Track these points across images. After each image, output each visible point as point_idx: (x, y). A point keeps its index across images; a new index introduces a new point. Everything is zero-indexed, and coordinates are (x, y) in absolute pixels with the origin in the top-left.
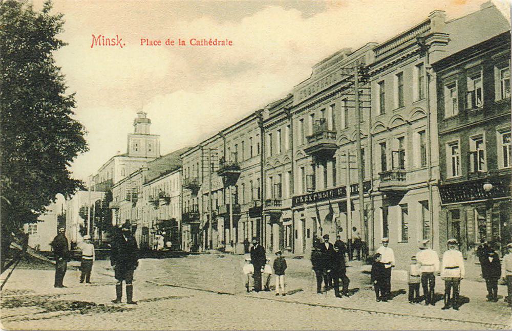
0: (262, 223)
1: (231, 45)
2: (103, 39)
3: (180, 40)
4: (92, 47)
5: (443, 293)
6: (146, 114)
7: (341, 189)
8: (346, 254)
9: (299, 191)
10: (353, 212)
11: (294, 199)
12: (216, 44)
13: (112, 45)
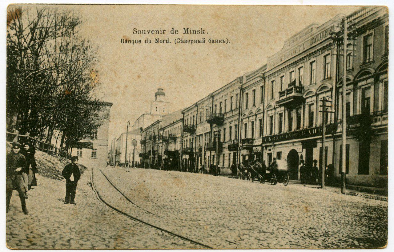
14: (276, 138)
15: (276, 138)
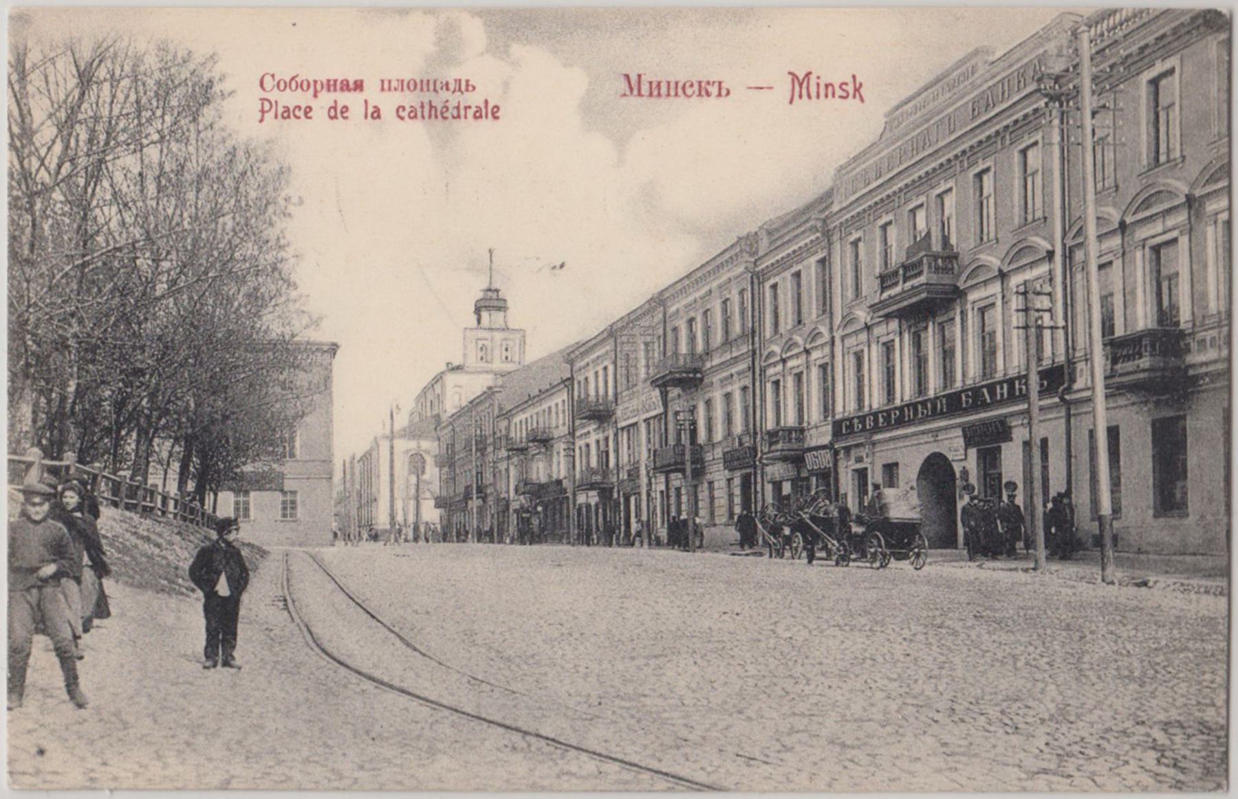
0: (756, 482)
1: (310, 118)
2: (818, 85)
3: (366, 102)
4: (791, 102)
5: (388, 527)
6: (497, 291)
7: (970, 393)
8: (866, 504)
9: (845, 405)
10: (1092, 427)
11: (837, 425)
12: (459, 117)
13: (841, 97)
14: (876, 420)
15: (876, 420)
